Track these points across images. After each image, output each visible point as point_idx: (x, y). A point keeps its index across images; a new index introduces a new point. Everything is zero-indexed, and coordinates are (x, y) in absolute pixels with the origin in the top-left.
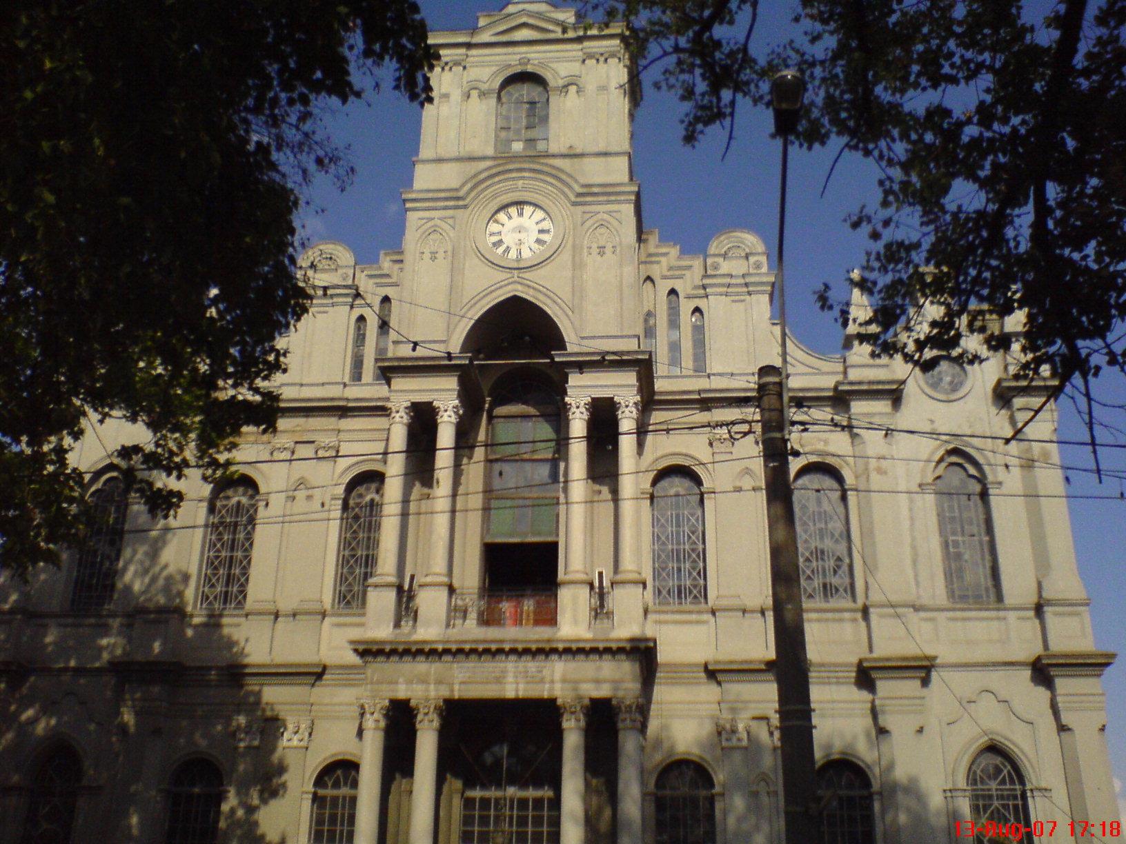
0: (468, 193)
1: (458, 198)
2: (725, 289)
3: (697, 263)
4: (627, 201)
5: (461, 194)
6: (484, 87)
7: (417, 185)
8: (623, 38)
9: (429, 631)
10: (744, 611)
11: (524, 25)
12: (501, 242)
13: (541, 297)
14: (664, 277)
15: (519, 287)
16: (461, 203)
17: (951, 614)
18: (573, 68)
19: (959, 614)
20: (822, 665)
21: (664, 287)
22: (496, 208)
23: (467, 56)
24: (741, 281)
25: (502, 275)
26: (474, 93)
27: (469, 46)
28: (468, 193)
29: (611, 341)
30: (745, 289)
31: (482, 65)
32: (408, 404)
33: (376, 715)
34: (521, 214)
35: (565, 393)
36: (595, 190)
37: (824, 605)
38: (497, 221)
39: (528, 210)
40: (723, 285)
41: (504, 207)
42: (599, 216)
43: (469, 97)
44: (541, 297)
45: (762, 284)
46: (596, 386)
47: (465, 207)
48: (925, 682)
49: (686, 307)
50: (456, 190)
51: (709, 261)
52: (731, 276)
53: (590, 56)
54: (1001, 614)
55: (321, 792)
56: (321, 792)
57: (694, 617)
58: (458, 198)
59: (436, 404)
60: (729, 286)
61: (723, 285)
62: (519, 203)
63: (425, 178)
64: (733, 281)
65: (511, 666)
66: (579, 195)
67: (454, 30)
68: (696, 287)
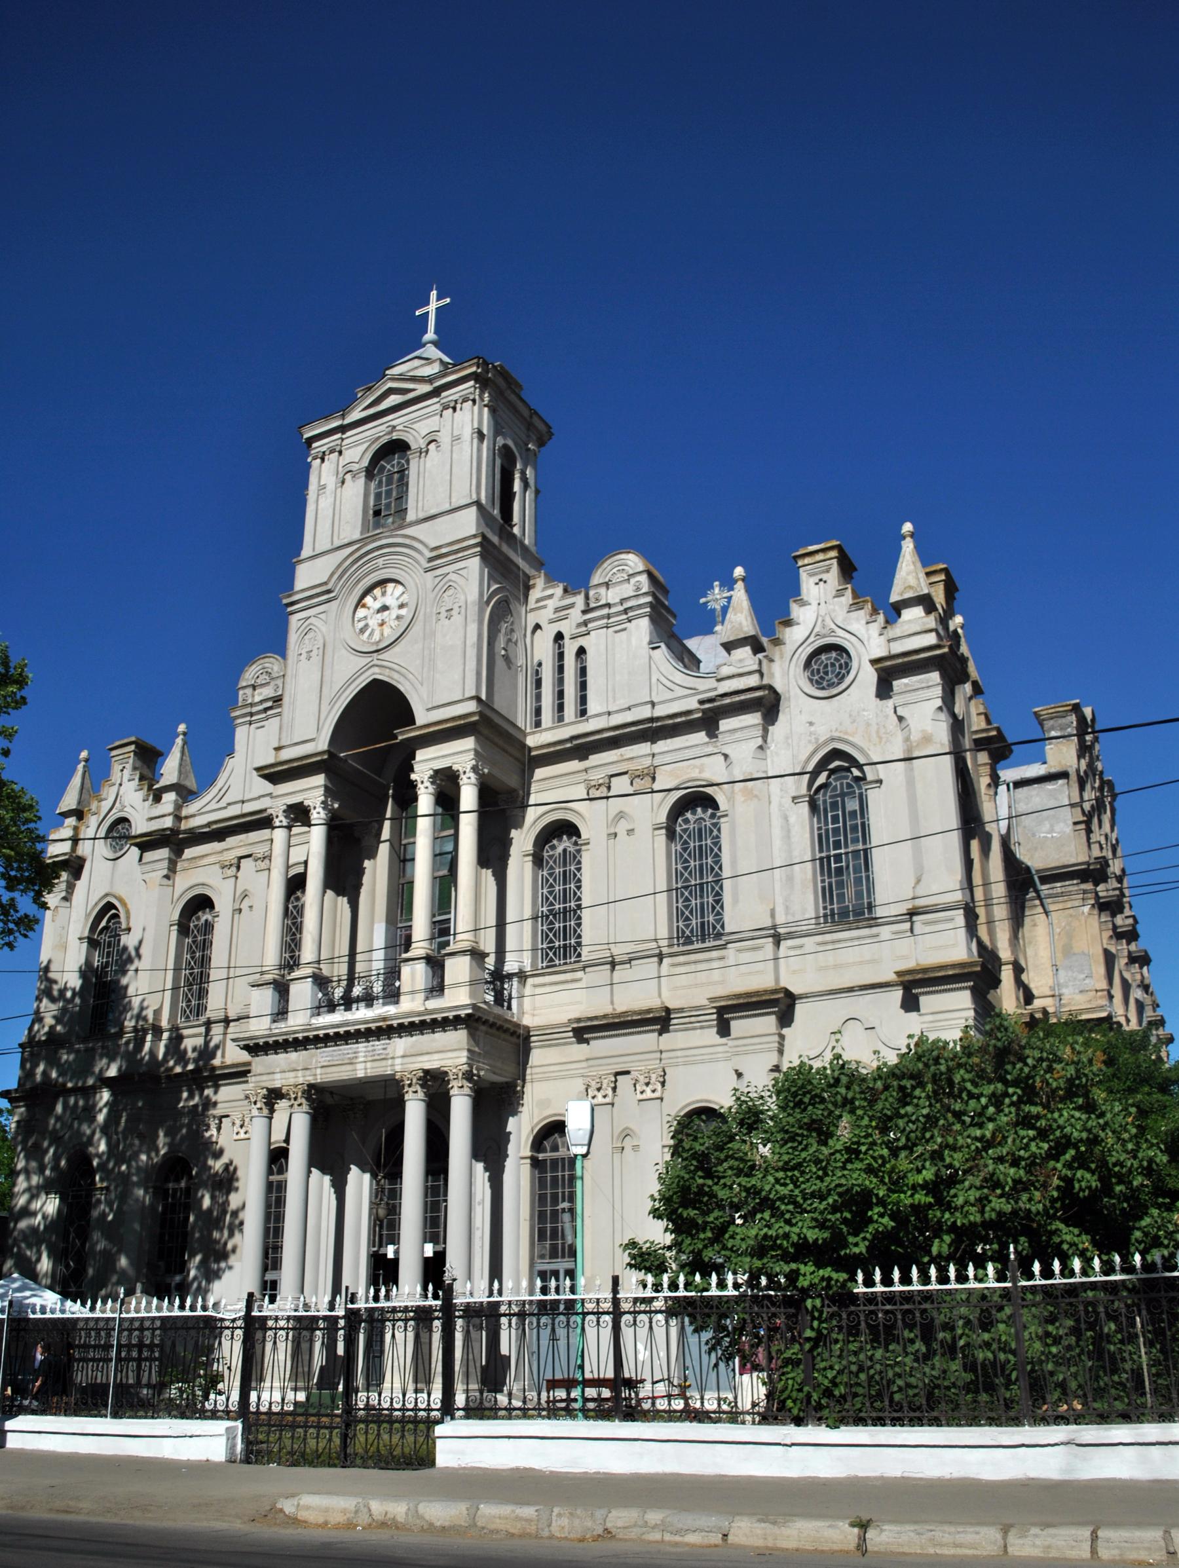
0: (336, 584)
1: (329, 592)
2: (605, 621)
3: (579, 600)
4: (474, 555)
5: (329, 587)
6: (355, 467)
7: (300, 584)
8: (474, 376)
9: (299, 1020)
10: (613, 964)
11: (391, 391)
12: (367, 626)
13: (396, 676)
14: (551, 622)
15: (376, 670)
16: (332, 595)
17: (819, 938)
18: (432, 424)
19: (828, 937)
20: (681, 1010)
21: (549, 632)
22: (360, 592)
23: (343, 440)
24: (621, 608)
25: (364, 661)
26: (348, 477)
27: (343, 429)
28: (336, 584)
29: (442, 710)
30: (625, 617)
31: (356, 444)
32: (285, 807)
33: (259, 1105)
34: (384, 594)
35: (412, 770)
36: (444, 551)
37: (700, 945)
38: (364, 606)
39: (390, 586)
40: (602, 617)
41: (368, 591)
42: (448, 577)
43: (343, 482)
44: (396, 676)
45: (640, 606)
46: (438, 758)
47: (334, 599)
48: (786, 1018)
49: (570, 649)
50: (325, 583)
51: (591, 593)
52: (608, 605)
53: (445, 407)
54: (875, 930)
55: (541, 1156)
56: (541, 1156)
57: (568, 976)
58: (329, 592)
59: (306, 803)
60: (609, 616)
61: (602, 617)
62: (383, 583)
63: (307, 576)
64: (613, 610)
65: (362, 1048)
66: (431, 560)
67: (326, 417)
68: (579, 625)
